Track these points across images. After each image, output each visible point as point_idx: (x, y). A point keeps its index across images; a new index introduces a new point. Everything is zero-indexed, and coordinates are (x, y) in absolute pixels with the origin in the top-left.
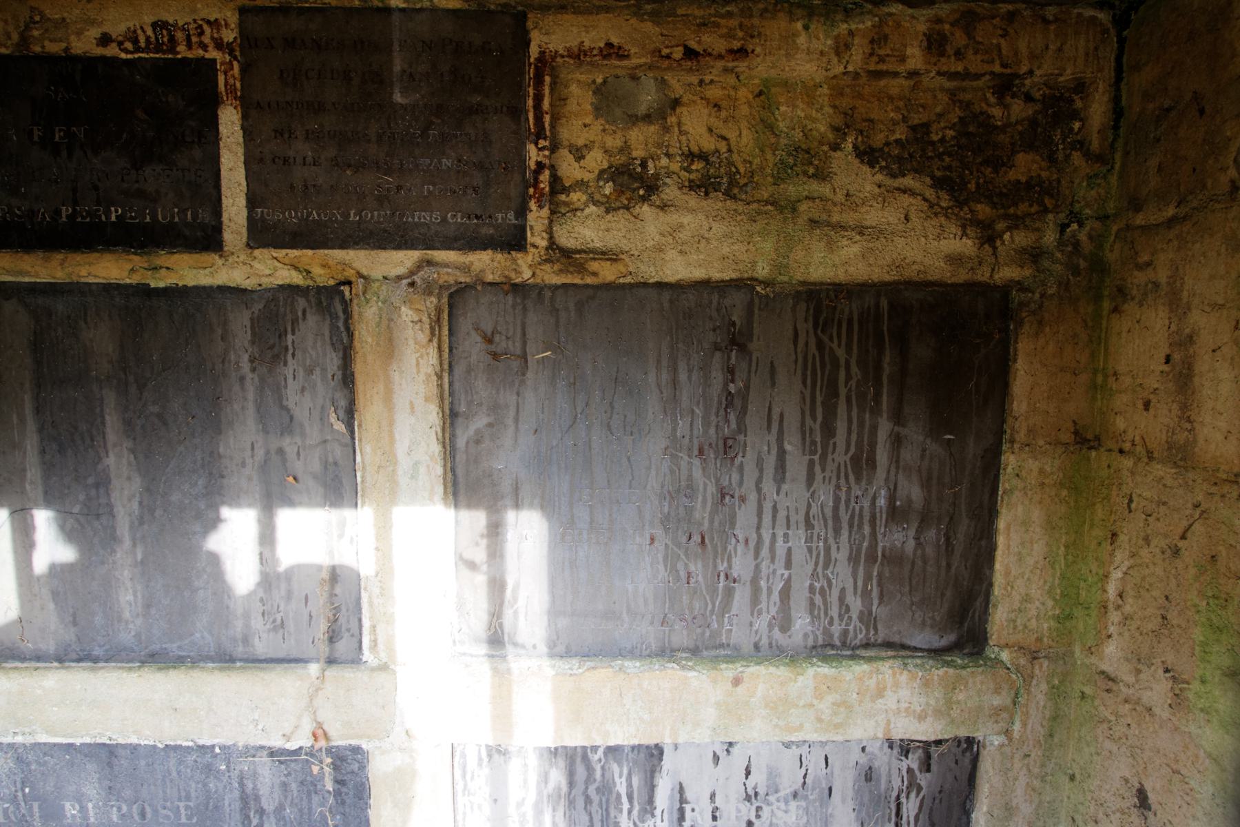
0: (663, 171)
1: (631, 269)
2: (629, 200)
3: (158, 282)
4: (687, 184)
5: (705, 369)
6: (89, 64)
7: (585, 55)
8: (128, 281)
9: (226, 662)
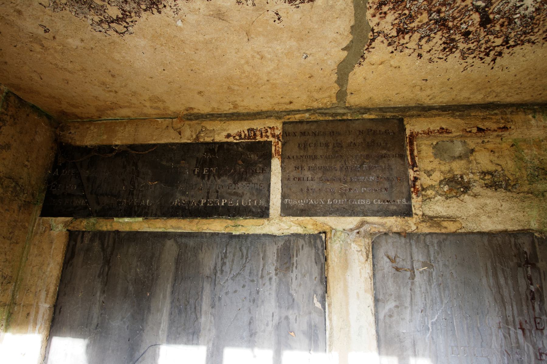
0: (472, 180)
1: (463, 225)
2: (456, 193)
3: (236, 232)
4: (484, 185)
5: (515, 278)
6: (221, 145)
7: (431, 133)
8: (223, 232)
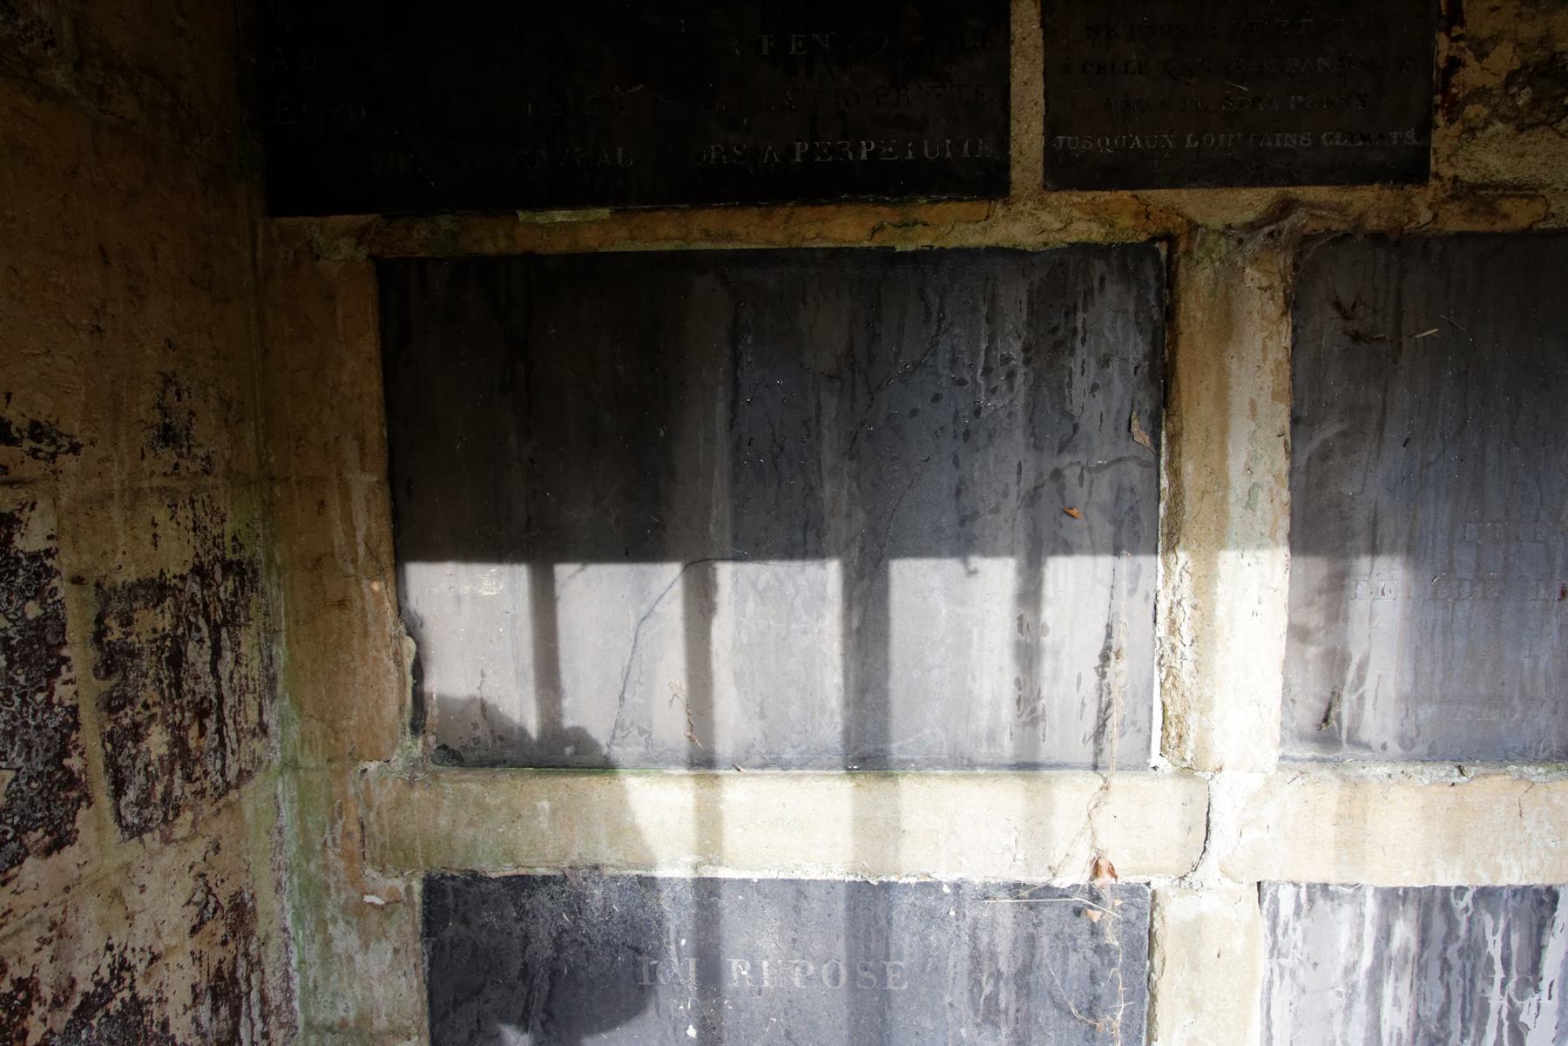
1: (1553, 210)
2: (1549, 113)
8: (866, 244)
9: (963, 767)
